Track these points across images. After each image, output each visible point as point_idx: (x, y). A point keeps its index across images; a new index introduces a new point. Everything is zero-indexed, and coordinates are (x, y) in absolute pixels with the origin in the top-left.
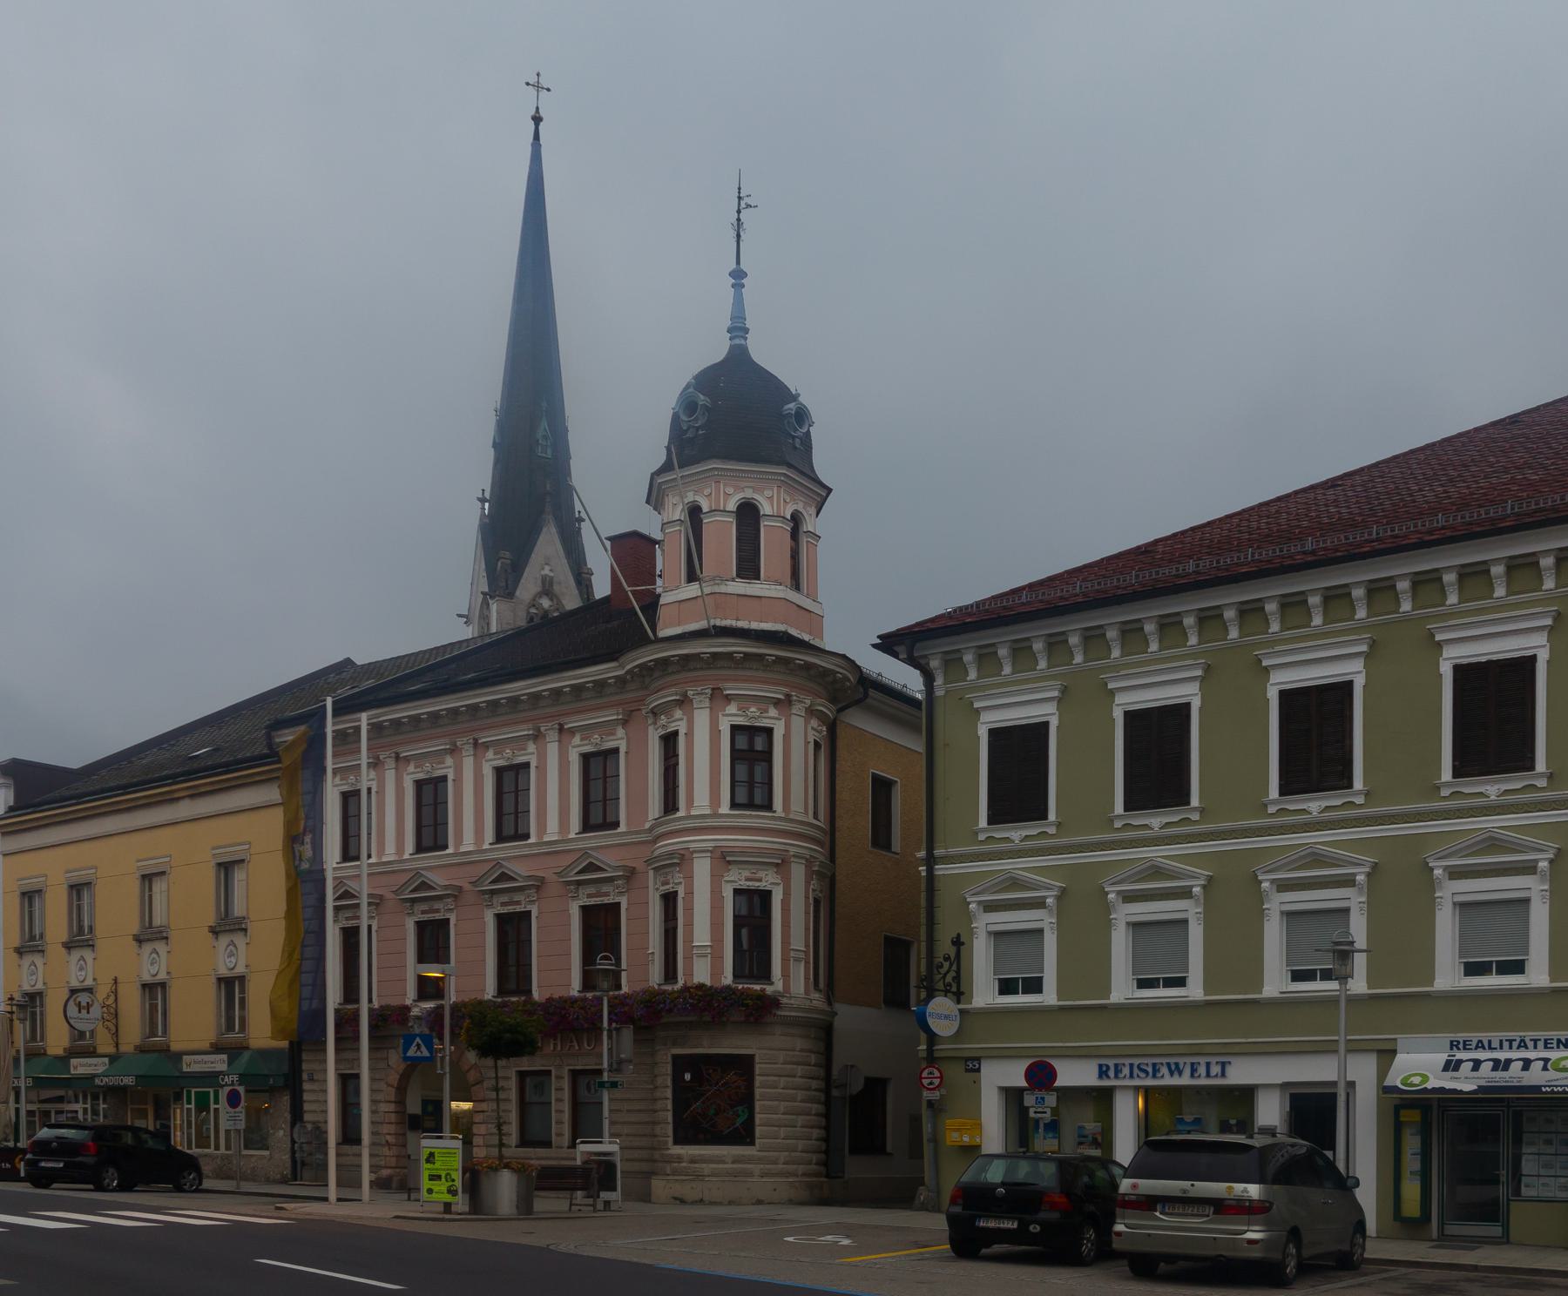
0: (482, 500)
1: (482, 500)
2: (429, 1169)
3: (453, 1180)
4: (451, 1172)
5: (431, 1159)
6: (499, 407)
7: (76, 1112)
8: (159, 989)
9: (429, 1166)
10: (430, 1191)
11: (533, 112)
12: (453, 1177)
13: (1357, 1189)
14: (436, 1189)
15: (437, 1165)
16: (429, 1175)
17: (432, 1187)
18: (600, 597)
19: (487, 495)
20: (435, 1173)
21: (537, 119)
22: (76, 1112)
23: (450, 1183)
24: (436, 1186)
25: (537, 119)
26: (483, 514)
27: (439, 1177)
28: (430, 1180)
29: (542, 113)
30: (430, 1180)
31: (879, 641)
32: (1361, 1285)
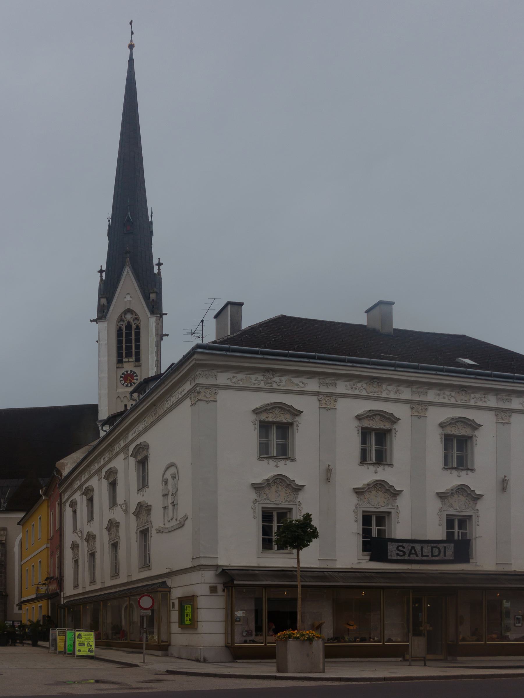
0: (101, 271)
1: (101, 271)
2: (79, 641)
3: (91, 646)
4: (90, 643)
5: (80, 636)
6: (111, 216)
7: (142, 618)
8: (230, 587)
9: (79, 639)
10: (79, 651)
11: (129, 42)
12: (91, 644)
13: (23, 622)
14: (82, 650)
15: (83, 639)
16: (79, 644)
17: (80, 649)
18: (105, 268)
19: (104, 268)
20: (82, 642)
21: (131, 46)
22: (142, 618)
23: (90, 647)
24: (82, 649)
25: (131, 46)
26: (101, 279)
27: (84, 645)
28: (79, 646)
29: (134, 42)
30: (79, 646)
31: (310, 517)
32: (169, 412)
